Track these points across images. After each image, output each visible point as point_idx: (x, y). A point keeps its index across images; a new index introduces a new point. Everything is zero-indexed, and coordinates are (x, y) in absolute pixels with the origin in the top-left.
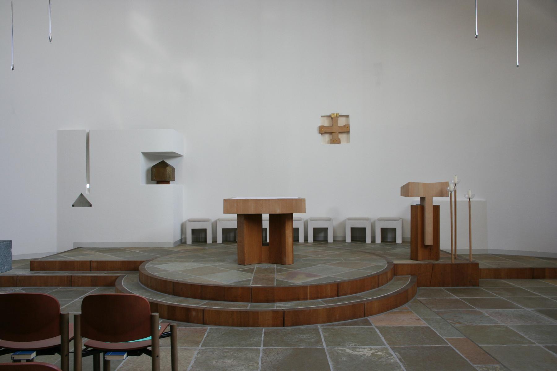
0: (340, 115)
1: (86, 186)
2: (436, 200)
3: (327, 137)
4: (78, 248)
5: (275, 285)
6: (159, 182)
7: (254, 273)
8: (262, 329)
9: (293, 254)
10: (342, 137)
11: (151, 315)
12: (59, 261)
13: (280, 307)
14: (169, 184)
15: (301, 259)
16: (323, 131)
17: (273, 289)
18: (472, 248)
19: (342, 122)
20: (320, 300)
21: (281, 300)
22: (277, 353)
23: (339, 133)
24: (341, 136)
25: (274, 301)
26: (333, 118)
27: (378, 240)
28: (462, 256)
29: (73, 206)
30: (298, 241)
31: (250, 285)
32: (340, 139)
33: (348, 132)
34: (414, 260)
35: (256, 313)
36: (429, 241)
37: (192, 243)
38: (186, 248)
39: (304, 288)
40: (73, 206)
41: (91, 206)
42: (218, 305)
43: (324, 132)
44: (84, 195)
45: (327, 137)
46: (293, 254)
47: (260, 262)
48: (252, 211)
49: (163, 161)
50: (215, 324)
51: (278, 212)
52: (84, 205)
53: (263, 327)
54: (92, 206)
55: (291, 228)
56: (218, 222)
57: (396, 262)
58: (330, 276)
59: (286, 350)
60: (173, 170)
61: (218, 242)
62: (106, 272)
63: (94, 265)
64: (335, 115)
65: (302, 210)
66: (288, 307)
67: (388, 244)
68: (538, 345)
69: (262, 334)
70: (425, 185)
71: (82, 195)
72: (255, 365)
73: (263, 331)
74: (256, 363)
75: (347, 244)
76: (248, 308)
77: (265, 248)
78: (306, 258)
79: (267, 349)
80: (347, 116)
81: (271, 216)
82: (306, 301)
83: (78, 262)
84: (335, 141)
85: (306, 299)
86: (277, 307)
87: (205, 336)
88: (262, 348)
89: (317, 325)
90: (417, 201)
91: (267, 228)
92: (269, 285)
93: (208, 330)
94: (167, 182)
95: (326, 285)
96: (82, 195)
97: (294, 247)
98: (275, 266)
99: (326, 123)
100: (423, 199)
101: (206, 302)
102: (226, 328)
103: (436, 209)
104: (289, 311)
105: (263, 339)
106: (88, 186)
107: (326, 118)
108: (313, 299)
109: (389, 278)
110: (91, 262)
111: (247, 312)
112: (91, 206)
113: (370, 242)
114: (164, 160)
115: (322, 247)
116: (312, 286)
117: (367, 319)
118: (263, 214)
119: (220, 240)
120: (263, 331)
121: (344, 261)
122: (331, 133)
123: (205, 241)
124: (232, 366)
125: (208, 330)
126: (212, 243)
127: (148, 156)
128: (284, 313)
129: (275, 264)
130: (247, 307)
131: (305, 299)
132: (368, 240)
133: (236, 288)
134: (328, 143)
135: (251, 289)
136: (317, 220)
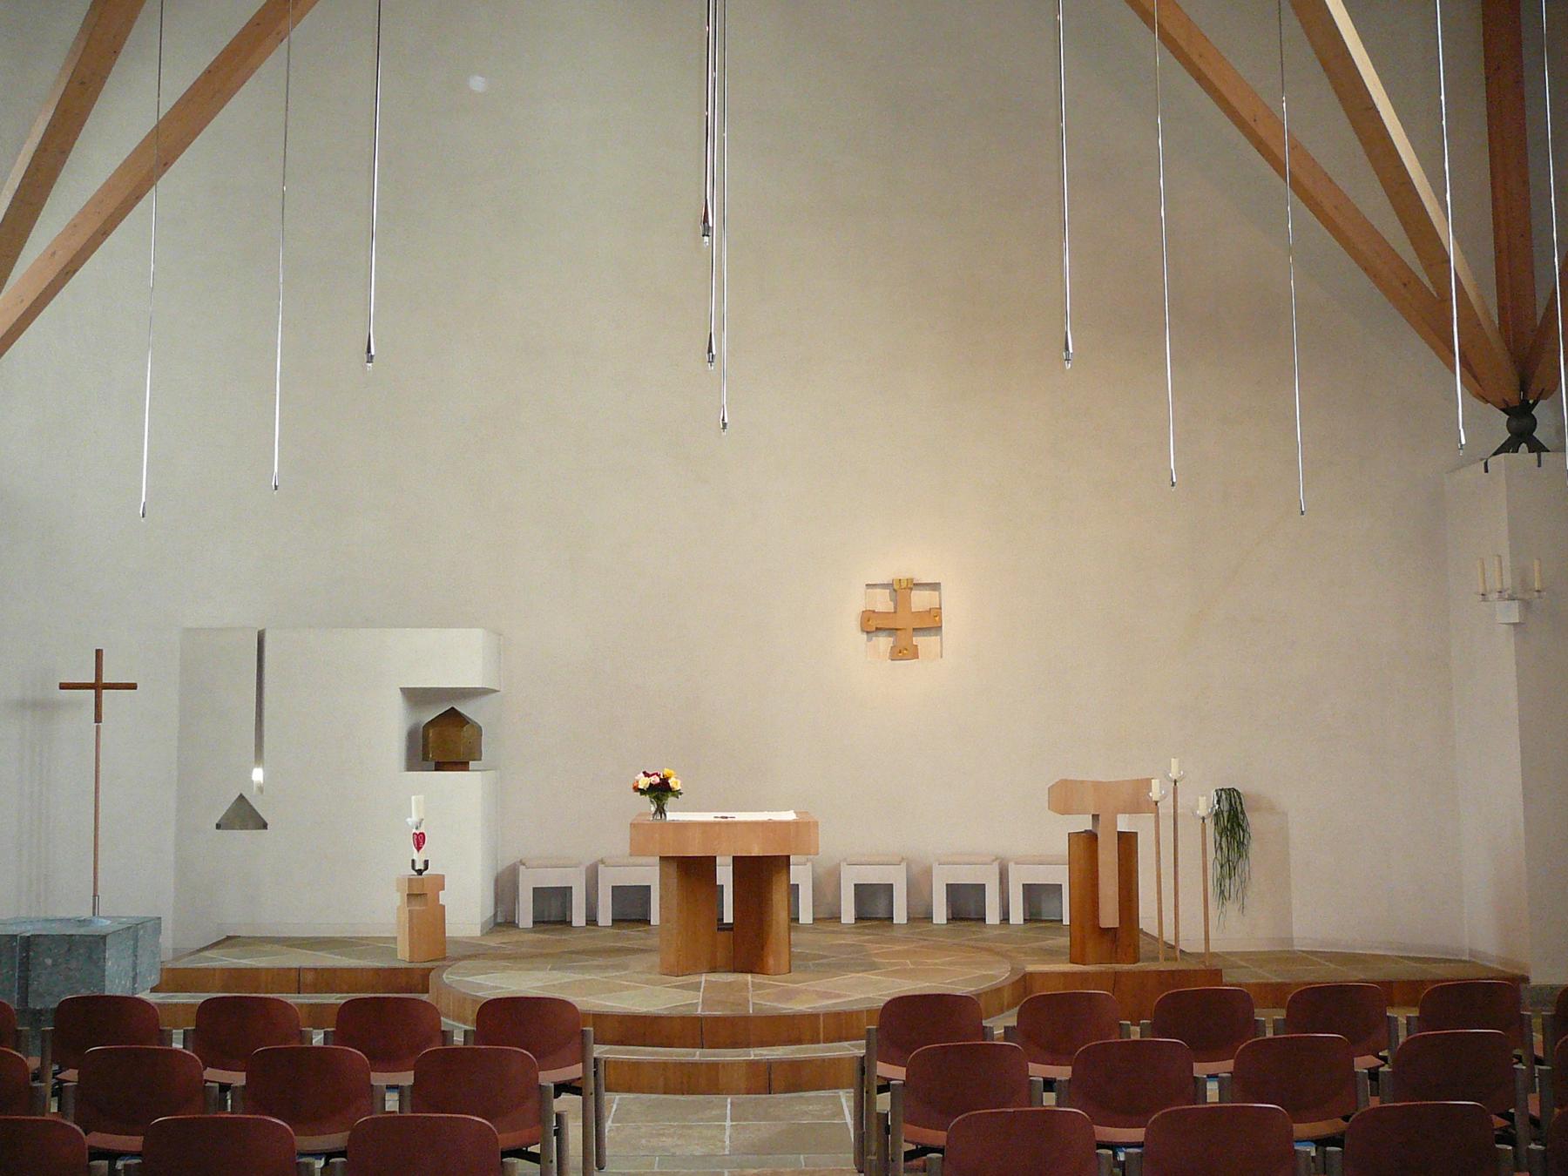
0: (915, 582)
2: (1124, 824)
4: (229, 938)
5: (751, 1012)
6: (439, 767)
7: (702, 990)
8: (727, 1099)
9: (790, 952)
11: (583, 1030)
12: (224, 970)
13: (761, 1055)
15: (810, 963)
16: (872, 625)
17: (746, 1019)
19: (920, 600)
20: (846, 1044)
21: (762, 1044)
22: (759, 1130)
24: (919, 640)
25: (748, 1046)
26: (901, 590)
27: (1017, 916)
29: (218, 826)
31: (699, 1011)
33: (937, 629)
34: (1077, 963)
35: (714, 1066)
36: (1109, 916)
38: (515, 938)
39: (813, 1018)
41: (265, 826)
42: (633, 1053)
43: (874, 629)
44: (247, 797)
45: (884, 642)
46: (790, 952)
47: (713, 970)
48: (695, 850)
49: (453, 708)
50: (629, 1091)
51: (756, 851)
53: (728, 1093)
54: (268, 827)
55: (784, 886)
56: (601, 867)
57: (1030, 968)
58: (871, 996)
59: (775, 1125)
60: (478, 730)
62: (339, 995)
63: (309, 977)
64: (904, 584)
65: (809, 850)
66: (778, 1055)
67: (1040, 928)
69: (727, 1106)
70: (1097, 785)
71: (241, 797)
72: (720, 1144)
73: (729, 1100)
74: (720, 1141)
75: (935, 927)
76: (697, 1058)
77: (723, 936)
78: (821, 961)
80: (935, 586)
81: (738, 862)
82: (817, 1046)
83: (267, 970)
84: (903, 652)
85: (819, 1042)
86: (755, 1055)
87: (614, 1110)
88: (728, 1123)
89: (837, 1091)
90: (1085, 823)
92: (739, 1012)
93: (616, 1101)
94: (462, 765)
95: (859, 1013)
96: (241, 797)
97: (792, 934)
98: (749, 977)
99: (882, 602)
100: (1095, 817)
101: (607, 1047)
102: (653, 1096)
103: (1127, 842)
104: (781, 1063)
105: (728, 1112)
106: (258, 775)
108: (832, 1042)
109: (1006, 1003)
110: (299, 970)
111: (694, 1064)
112: (265, 826)
114: (455, 707)
115: (868, 935)
116: (827, 1015)
119: (605, 917)
120: (729, 1100)
121: (908, 961)
122: (892, 631)
124: (677, 1145)
125: (616, 1101)
126: (587, 924)
127: (415, 697)
128: (769, 1065)
129: (748, 973)
130: (694, 1056)
131: (815, 1041)
132: (993, 917)
133: (669, 1019)
135: (699, 1020)
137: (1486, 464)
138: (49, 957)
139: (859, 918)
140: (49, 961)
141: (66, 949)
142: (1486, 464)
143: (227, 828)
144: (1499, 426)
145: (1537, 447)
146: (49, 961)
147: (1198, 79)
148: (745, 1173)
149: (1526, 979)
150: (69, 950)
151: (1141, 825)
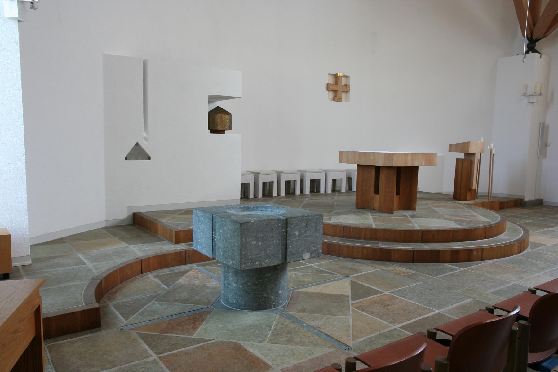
1: (488, 148)
10: (343, 95)
14: (225, 133)
16: (328, 87)
23: (343, 91)
28: (165, 224)
29: (126, 159)
30: (318, 191)
37: (263, 197)
40: (126, 159)
41: (149, 158)
43: (331, 90)
52: (137, 158)
54: (151, 158)
68: (312, 265)
71: (137, 144)
80: (346, 77)
90: (461, 156)
91: (273, 182)
96: (137, 144)
112: (149, 158)
117: (43, 319)
134: (332, 100)
136: (471, 166)
140: (297, 233)
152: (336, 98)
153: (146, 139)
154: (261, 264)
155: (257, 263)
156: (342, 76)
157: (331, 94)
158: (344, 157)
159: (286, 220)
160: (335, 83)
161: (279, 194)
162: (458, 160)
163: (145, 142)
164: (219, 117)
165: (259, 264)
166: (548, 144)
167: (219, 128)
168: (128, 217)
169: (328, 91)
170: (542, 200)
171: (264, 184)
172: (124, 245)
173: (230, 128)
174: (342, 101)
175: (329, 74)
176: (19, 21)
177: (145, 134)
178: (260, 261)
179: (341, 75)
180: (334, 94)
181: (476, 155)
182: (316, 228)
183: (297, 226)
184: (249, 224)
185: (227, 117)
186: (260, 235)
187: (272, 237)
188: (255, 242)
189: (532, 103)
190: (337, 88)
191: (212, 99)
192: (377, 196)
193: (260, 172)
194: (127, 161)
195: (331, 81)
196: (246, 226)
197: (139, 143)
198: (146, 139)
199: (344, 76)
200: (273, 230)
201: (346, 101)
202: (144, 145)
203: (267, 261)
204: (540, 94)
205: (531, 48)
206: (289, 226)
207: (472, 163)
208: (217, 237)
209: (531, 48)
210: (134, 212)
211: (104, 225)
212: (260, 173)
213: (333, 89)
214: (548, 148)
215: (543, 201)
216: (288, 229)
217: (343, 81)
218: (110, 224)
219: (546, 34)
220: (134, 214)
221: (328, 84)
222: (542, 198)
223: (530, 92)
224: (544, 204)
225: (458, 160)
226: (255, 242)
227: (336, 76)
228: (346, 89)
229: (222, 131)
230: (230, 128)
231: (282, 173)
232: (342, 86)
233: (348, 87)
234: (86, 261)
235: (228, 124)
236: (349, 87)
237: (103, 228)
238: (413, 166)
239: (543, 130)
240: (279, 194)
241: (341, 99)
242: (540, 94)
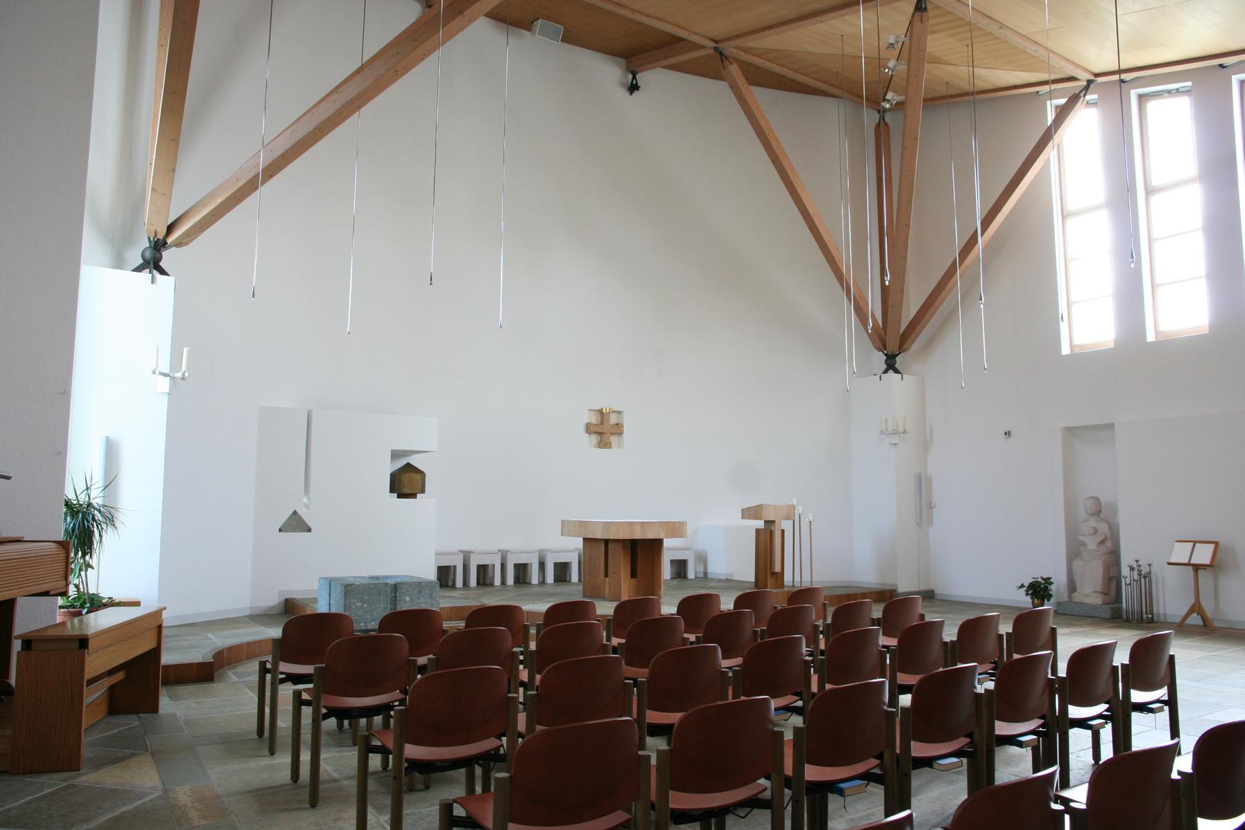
3: (595, 438)
10: (614, 439)
16: (589, 429)
18: (814, 580)
19: (613, 419)
23: (612, 434)
29: (280, 530)
32: (611, 443)
33: (620, 433)
40: (280, 530)
41: (309, 530)
44: (300, 513)
61: (496, 584)
71: (295, 513)
79: (951, 651)
80: (619, 413)
90: (760, 524)
96: (295, 513)
99: (594, 419)
107: (593, 412)
112: (309, 530)
113: (669, 578)
118: (664, 540)
123: (492, 585)
134: (595, 447)
137: (880, 377)
138: (408, 595)
139: (478, 583)
140: (408, 599)
141: (417, 591)
142: (880, 377)
143: (286, 531)
144: (880, 358)
145: (897, 371)
146: (408, 599)
147: (791, 193)
148: (516, 712)
149: (895, 591)
150: (419, 591)
151: (786, 525)
152: (604, 444)
153: (307, 506)
154: (367, 626)
155: (362, 624)
156: (609, 412)
157: (594, 439)
158: (568, 528)
159: (395, 585)
160: (600, 423)
161: (503, 582)
162: (758, 531)
163: (305, 510)
164: (406, 477)
165: (365, 626)
166: (933, 506)
167: (406, 491)
168: (279, 603)
169: (589, 434)
170: (933, 591)
171: (479, 567)
172: (263, 628)
173: (423, 491)
174: (611, 447)
175: (590, 410)
176: (169, 394)
177: (305, 500)
178: (365, 623)
179: (608, 411)
180: (599, 437)
181: (776, 522)
182: (431, 595)
183: (408, 591)
184: (354, 586)
185: (418, 476)
186: (365, 598)
187: (379, 600)
188: (360, 604)
189: (896, 444)
190: (605, 429)
191: (396, 455)
192: (607, 579)
193: (472, 550)
194: (281, 533)
195: (594, 419)
196: (350, 588)
197: (297, 511)
198: (307, 506)
199: (614, 412)
200: (379, 593)
201: (619, 447)
202: (303, 513)
203: (373, 623)
204: (905, 432)
205: (891, 365)
206: (398, 591)
207: (771, 533)
208: (331, 602)
209: (891, 365)
210: (287, 597)
211: (247, 613)
212: (472, 552)
213: (597, 431)
214: (934, 510)
215: (936, 592)
216: (398, 594)
217: (613, 419)
218: (254, 612)
219: (904, 348)
220: (287, 601)
221: (587, 424)
222: (933, 589)
223: (891, 428)
224: (937, 597)
225: (758, 531)
226: (360, 604)
227: (601, 412)
228: (618, 429)
229: (413, 496)
230: (423, 491)
231: (509, 553)
232: (611, 425)
233: (620, 426)
234: (213, 638)
235: (420, 487)
236: (622, 426)
237: (246, 616)
238: (644, 538)
239: (922, 486)
240: (503, 582)
241: (609, 445)
242: (905, 432)
